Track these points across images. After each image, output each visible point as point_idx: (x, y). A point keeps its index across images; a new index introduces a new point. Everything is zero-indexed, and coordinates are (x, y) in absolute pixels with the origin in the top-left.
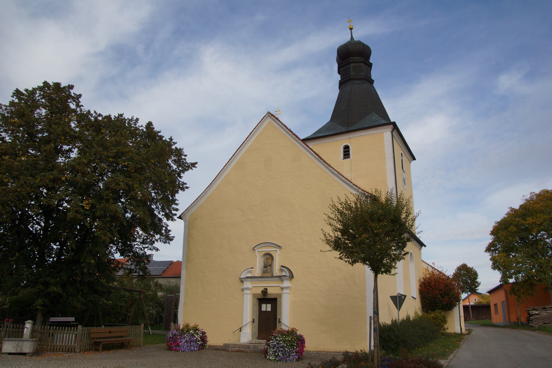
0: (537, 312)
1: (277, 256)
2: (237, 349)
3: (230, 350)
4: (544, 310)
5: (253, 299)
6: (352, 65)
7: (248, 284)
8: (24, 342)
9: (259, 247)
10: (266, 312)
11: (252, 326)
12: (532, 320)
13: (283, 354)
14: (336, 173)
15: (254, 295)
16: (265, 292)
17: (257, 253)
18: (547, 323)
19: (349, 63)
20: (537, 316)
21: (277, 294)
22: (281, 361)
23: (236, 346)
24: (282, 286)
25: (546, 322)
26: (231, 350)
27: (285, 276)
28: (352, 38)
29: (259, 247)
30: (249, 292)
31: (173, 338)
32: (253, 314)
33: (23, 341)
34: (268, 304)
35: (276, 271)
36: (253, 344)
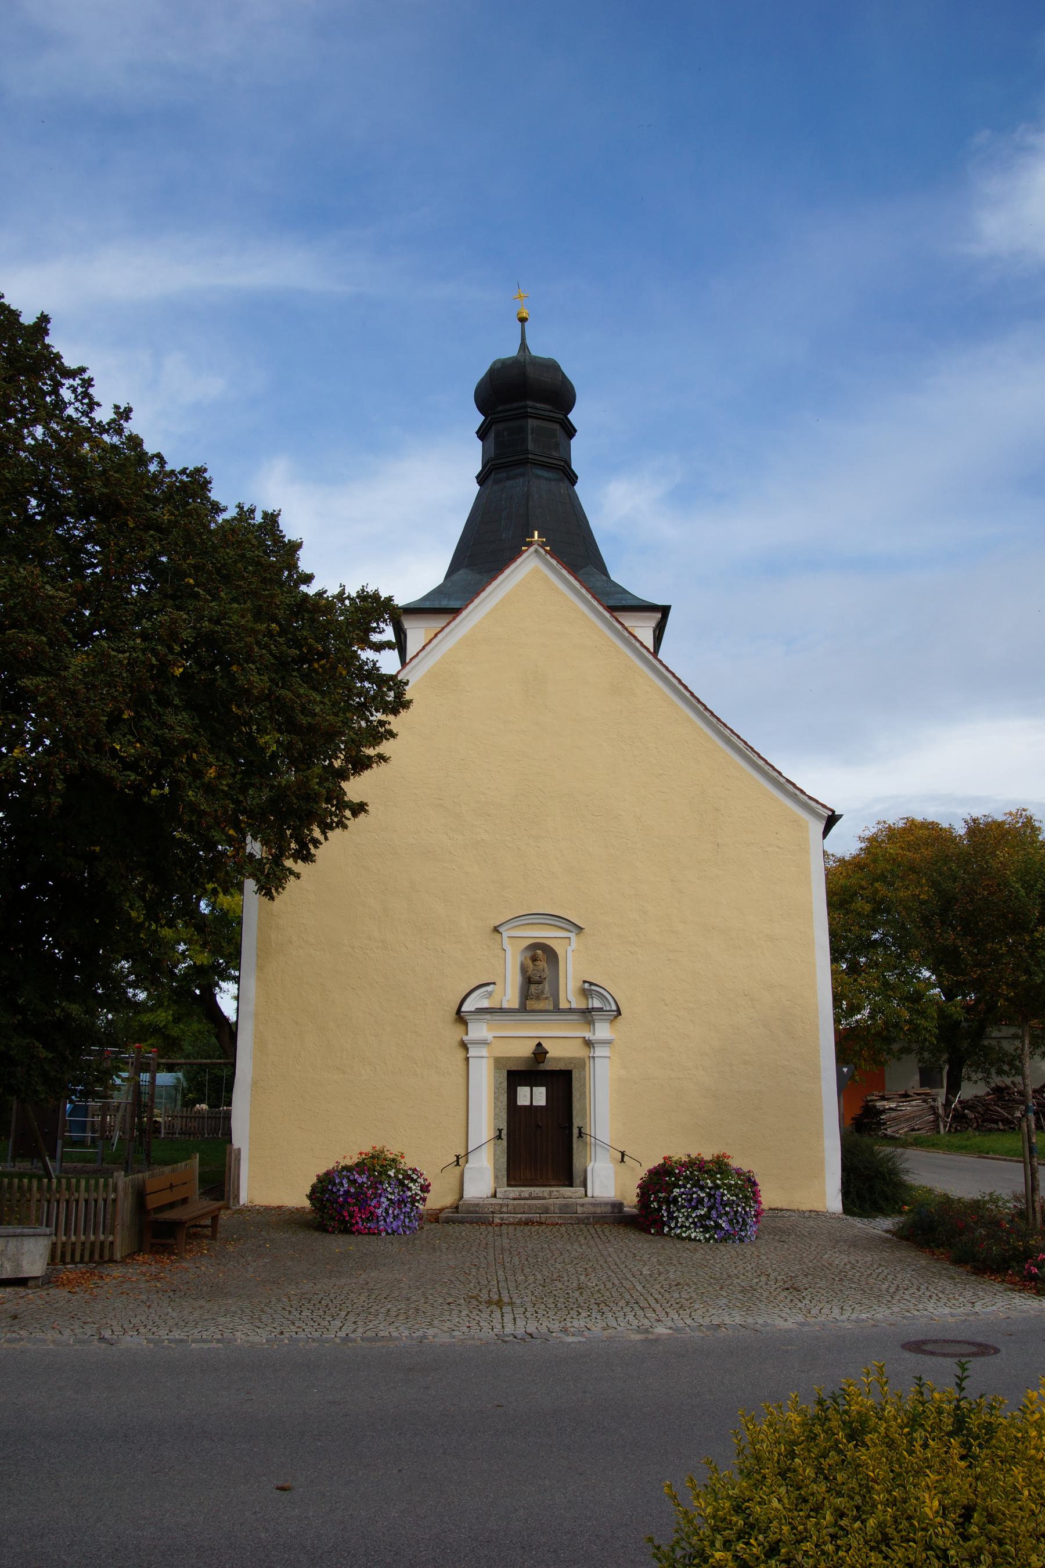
0: (893, 1105)
1: (570, 955)
2: (519, 1216)
3: (497, 1221)
4: (903, 1100)
5: (495, 1072)
6: (532, 423)
7: (479, 1030)
8: (24, 1238)
9: (514, 924)
10: (531, 1108)
11: (495, 1151)
12: (885, 1124)
13: (730, 1222)
14: (741, 745)
15: (498, 1062)
16: (540, 1053)
17: (506, 940)
18: (918, 1130)
19: (526, 416)
20: (894, 1114)
21: (572, 1058)
22: (726, 1240)
23: (504, 1209)
24: (588, 1035)
25: (916, 1127)
26: (499, 1221)
27: (601, 1010)
28: (523, 346)
29: (514, 924)
30: (484, 1052)
31: (357, 1195)
32: (496, 1115)
33: (19, 1239)
34: (536, 1086)
35: (569, 995)
36: (522, 1202)
